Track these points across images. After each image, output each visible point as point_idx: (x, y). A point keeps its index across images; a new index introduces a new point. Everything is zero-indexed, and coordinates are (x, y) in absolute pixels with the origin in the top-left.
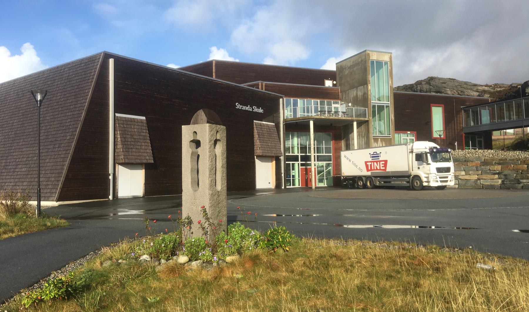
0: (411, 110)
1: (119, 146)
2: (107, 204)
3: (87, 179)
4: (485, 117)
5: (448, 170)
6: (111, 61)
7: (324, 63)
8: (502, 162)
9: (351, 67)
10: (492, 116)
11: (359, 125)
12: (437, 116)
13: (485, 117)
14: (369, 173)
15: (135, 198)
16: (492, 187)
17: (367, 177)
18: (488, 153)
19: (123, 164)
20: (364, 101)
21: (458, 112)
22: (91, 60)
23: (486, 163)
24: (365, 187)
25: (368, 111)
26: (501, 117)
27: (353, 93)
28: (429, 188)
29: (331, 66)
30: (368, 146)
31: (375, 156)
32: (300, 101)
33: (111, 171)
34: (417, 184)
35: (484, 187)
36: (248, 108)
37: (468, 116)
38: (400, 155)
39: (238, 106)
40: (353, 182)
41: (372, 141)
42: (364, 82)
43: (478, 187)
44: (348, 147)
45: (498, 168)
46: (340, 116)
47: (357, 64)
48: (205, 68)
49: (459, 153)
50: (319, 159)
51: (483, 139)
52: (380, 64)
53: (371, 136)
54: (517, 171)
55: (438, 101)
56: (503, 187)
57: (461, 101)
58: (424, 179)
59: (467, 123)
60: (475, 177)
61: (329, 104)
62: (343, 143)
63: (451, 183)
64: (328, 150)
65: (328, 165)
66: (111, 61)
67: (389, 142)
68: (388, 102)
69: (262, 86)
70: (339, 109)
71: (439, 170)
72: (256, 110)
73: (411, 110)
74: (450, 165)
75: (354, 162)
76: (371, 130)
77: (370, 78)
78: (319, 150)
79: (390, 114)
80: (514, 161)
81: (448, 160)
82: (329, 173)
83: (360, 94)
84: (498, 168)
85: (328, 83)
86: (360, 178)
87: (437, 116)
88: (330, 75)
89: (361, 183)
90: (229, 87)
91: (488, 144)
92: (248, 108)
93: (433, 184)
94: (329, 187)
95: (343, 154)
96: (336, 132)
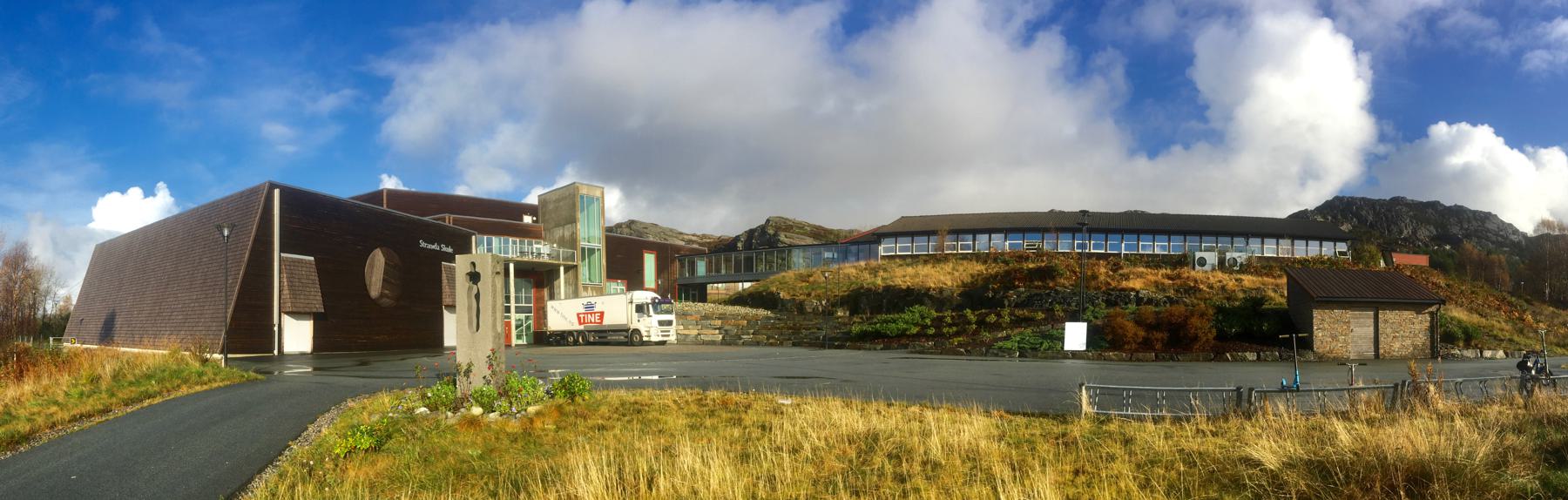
0: (623, 255)
1: (286, 292)
2: (271, 359)
3: (250, 331)
4: (701, 268)
5: (669, 323)
6: (277, 192)
7: (526, 195)
8: (722, 317)
9: (558, 201)
10: (709, 269)
11: (566, 271)
12: (650, 261)
13: (701, 268)
14: (582, 327)
15: (303, 354)
16: (713, 343)
17: (579, 332)
18: (707, 307)
19: (292, 314)
20: (572, 242)
21: (673, 261)
22: (254, 192)
23: (706, 317)
24: (576, 343)
25: (578, 254)
26: (718, 271)
27: (558, 233)
28: (649, 343)
29: (532, 199)
30: (576, 295)
31: (589, 307)
32: (495, 240)
33: (276, 321)
34: (636, 338)
35: (705, 343)
36: (435, 247)
37: (682, 266)
38: (617, 307)
39: (423, 244)
40: (562, 338)
41: (581, 288)
42: (572, 220)
43: (698, 342)
44: (552, 297)
45: (718, 323)
46: (546, 259)
47: (564, 198)
48: (376, 197)
49: (678, 305)
50: (518, 310)
51: (697, 292)
52: (591, 200)
53: (581, 282)
54: (737, 326)
55: (651, 247)
56: (724, 342)
57: (677, 249)
58: (644, 334)
59: (682, 274)
60: (695, 332)
61: (530, 244)
62: (546, 292)
63: (672, 338)
64: (528, 300)
65: (527, 318)
66: (277, 192)
67: (600, 291)
68: (599, 244)
69: (449, 220)
70: (543, 250)
71: (661, 323)
72: (445, 249)
73: (623, 255)
74: (672, 317)
75: (562, 314)
76: (581, 277)
77: (579, 215)
78: (517, 300)
79: (600, 260)
80: (735, 316)
81: (670, 312)
82: (528, 327)
83: (567, 234)
84: (718, 323)
85: (527, 219)
86: (570, 333)
87: (650, 261)
88: (532, 210)
89: (571, 339)
90: (410, 221)
91: (703, 298)
92: (435, 247)
93: (654, 339)
94: (528, 345)
95: (550, 304)
96: (538, 277)
